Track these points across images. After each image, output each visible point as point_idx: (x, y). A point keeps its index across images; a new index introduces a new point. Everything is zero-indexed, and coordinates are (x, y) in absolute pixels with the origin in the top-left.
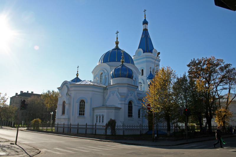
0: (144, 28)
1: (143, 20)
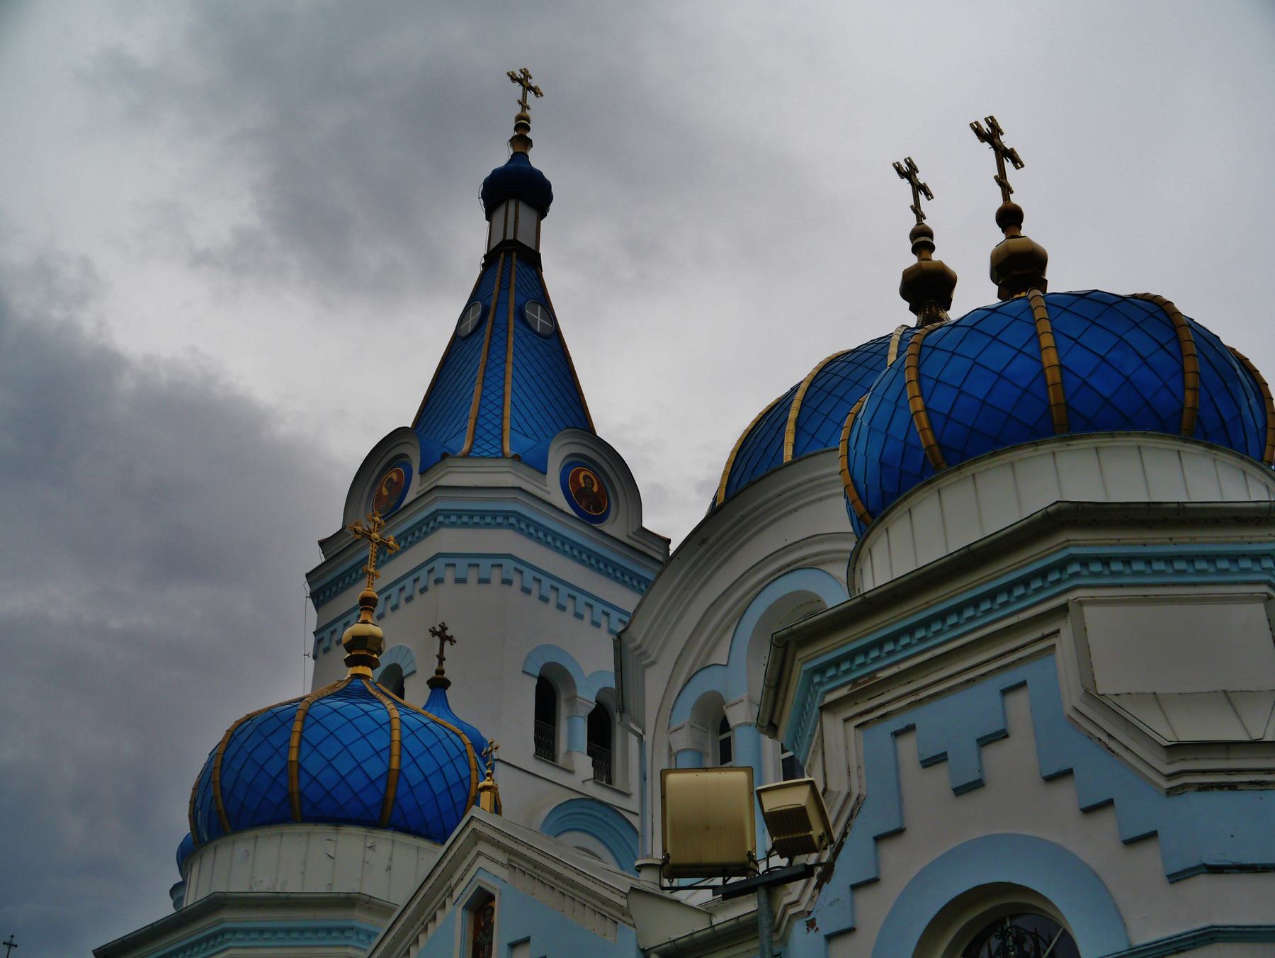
0: (497, 240)
1: (501, 156)
